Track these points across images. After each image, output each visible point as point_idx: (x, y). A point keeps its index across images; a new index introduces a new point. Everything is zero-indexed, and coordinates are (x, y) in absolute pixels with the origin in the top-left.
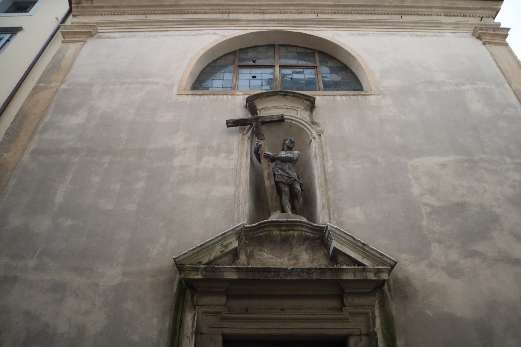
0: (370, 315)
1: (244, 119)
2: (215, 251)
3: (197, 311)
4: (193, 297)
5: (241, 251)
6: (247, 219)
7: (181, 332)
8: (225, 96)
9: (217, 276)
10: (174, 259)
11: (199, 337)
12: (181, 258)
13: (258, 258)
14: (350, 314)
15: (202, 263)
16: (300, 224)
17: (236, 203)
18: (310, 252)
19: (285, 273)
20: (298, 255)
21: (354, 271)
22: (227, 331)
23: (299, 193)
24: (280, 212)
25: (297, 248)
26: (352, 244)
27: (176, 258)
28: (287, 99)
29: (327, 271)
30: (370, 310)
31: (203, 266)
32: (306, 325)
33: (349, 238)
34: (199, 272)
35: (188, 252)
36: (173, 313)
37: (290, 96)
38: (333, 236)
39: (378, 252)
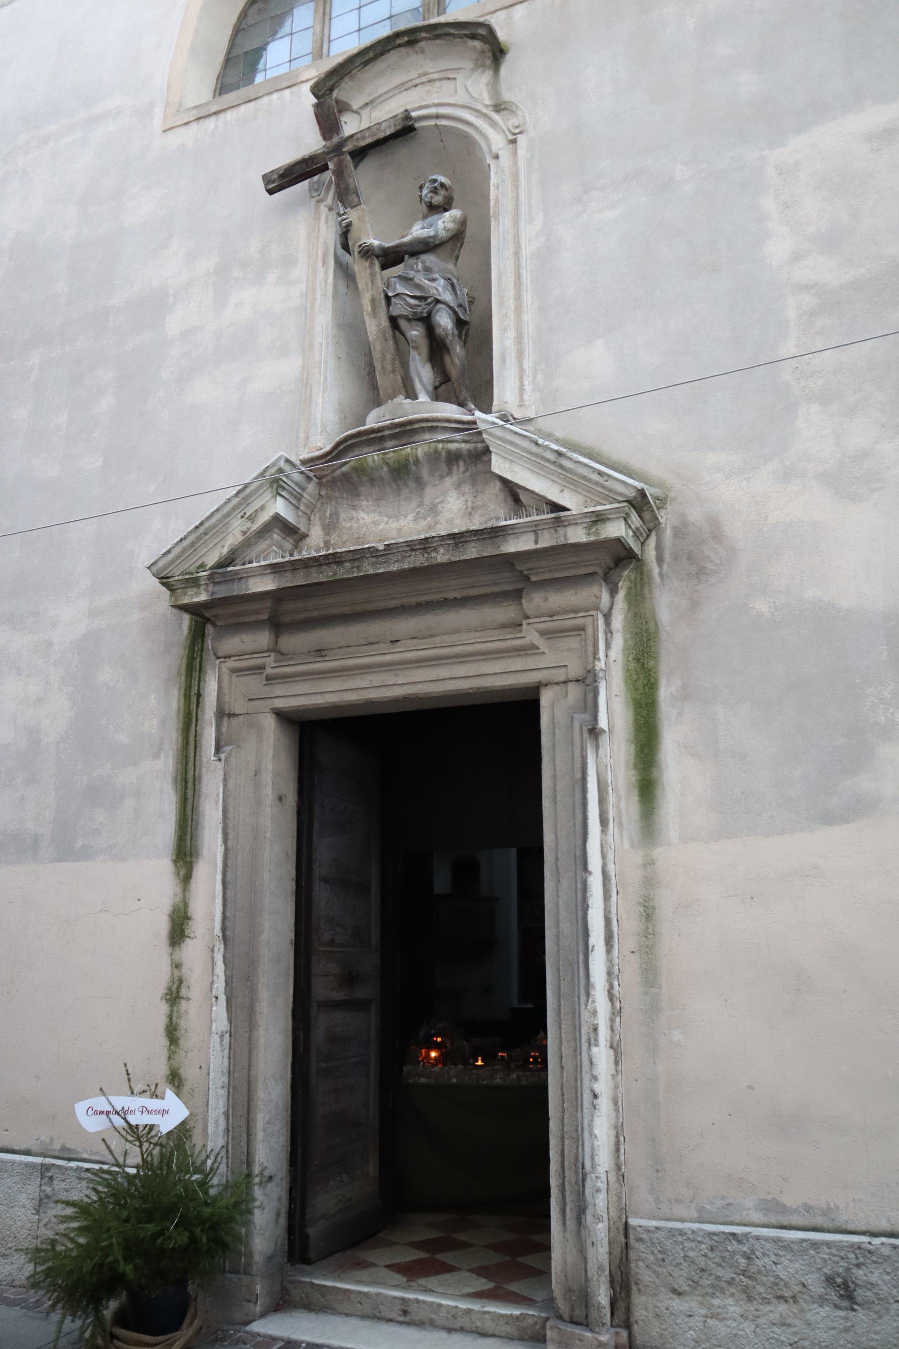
1: (307, 157)
2: (231, 534)
7: (199, 717)
8: (275, 96)
9: (237, 590)
12: (161, 564)
15: (206, 565)
18: (467, 489)
19: (374, 560)
20: (438, 503)
21: (535, 529)
22: (281, 704)
24: (403, 397)
25: (435, 486)
26: (532, 458)
28: (422, 51)
29: (468, 539)
31: (205, 573)
32: (443, 672)
34: (202, 588)
35: (171, 548)
36: (183, 678)
37: (425, 39)
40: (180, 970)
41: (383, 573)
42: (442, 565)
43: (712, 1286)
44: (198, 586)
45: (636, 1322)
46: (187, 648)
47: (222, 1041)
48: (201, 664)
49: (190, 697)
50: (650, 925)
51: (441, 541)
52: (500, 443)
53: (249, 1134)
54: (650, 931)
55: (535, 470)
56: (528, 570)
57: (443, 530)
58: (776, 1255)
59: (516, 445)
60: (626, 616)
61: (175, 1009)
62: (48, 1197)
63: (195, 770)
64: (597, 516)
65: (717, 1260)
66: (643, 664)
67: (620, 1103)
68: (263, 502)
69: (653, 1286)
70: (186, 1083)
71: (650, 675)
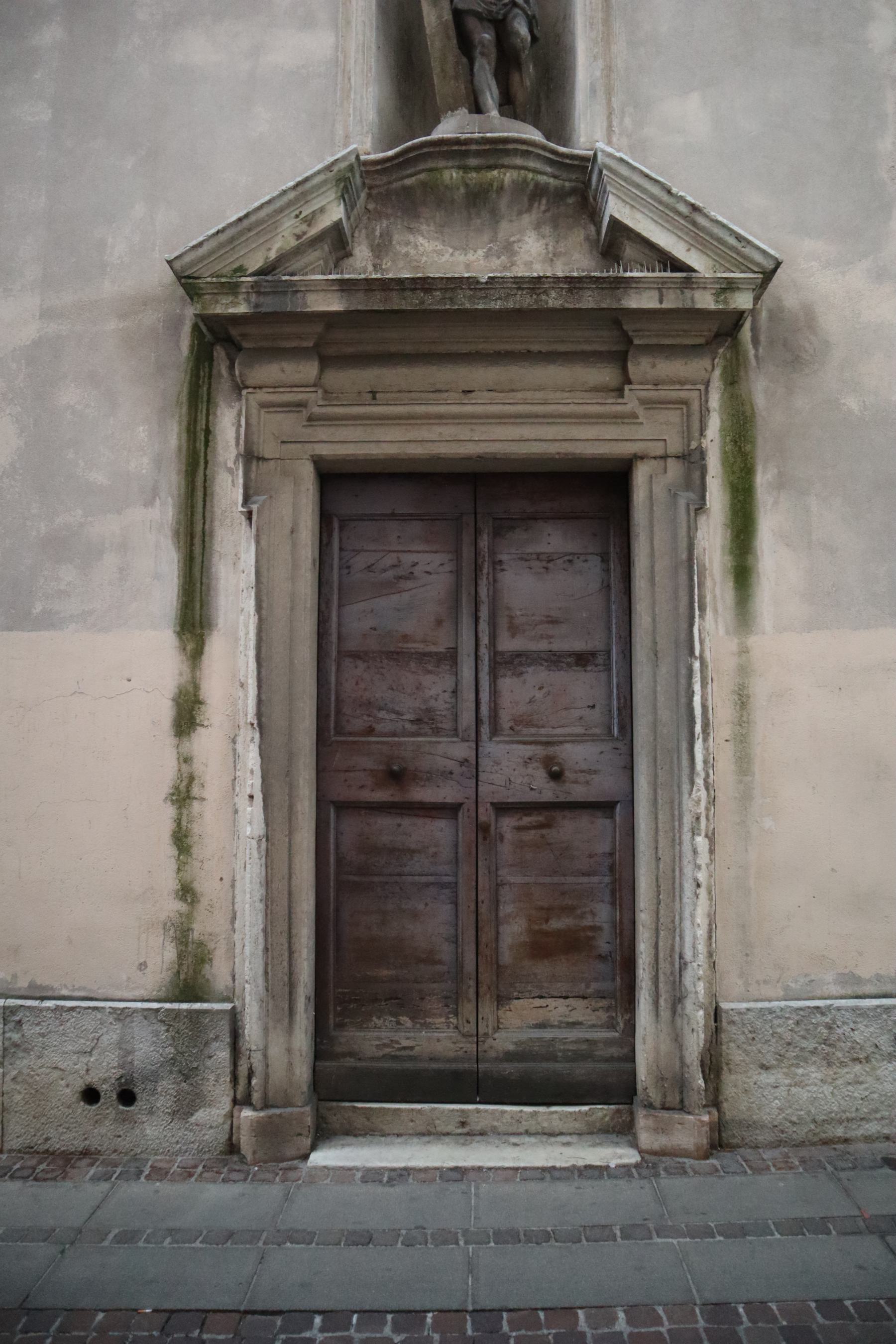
0: (695, 406)
2: (280, 236)
3: (244, 401)
4: (231, 367)
5: (356, 235)
6: (373, 137)
7: (209, 458)
9: (289, 305)
10: (169, 262)
11: (254, 467)
12: (187, 259)
13: (403, 251)
14: (643, 402)
15: (247, 270)
16: (519, 147)
17: (339, 86)
19: (472, 293)
20: (514, 242)
21: (661, 287)
22: (325, 450)
23: (524, 48)
24: (466, 111)
25: (511, 221)
27: (173, 260)
29: (585, 285)
30: (697, 393)
31: (249, 279)
32: (526, 431)
33: (655, 190)
34: (241, 297)
35: (204, 241)
38: (609, 183)
39: (732, 232)
40: (190, 765)
41: (481, 310)
42: (554, 310)
43: (797, 1057)
44: (235, 294)
45: (726, 1100)
46: (189, 371)
47: (259, 847)
48: (209, 394)
49: (195, 433)
50: (745, 713)
51: (555, 283)
52: (623, 183)
53: (291, 952)
54: (744, 719)
55: (660, 221)
56: (634, 331)
57: (520, 271)
58: (854, 1022)
59: (644, 190)
60: (722, 395)
61: (185, 812)
62: (16, 1045)
63: (204, 523)
64: (728, 283)
65: (802, 1033)
66: (740, 447)
67: (713, 893)
68: (323, 203)
69: (743, 1064)
70: (202, 899)
71: (746, 459)
